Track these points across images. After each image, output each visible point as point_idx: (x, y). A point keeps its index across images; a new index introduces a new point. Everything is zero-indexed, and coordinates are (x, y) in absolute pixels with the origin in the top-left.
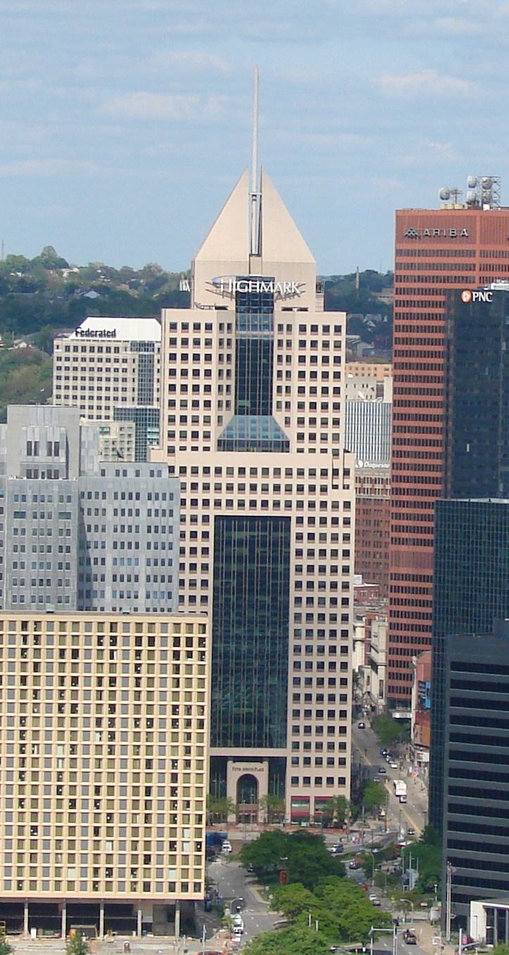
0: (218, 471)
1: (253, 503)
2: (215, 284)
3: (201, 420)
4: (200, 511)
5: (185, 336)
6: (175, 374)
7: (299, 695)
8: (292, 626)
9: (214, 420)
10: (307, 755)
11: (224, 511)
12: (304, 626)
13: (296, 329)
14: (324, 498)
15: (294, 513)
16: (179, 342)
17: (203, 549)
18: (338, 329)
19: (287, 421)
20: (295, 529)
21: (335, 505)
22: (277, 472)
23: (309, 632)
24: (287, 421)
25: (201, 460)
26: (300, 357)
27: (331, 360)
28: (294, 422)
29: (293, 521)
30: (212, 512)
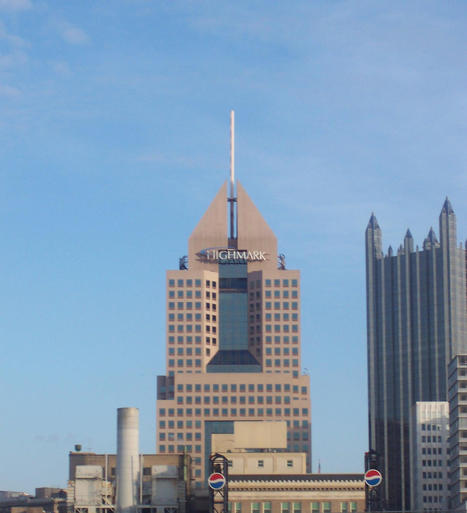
11: (212, 418)
14: (287, 406)
25: (194, 380)
30: (203, 418)
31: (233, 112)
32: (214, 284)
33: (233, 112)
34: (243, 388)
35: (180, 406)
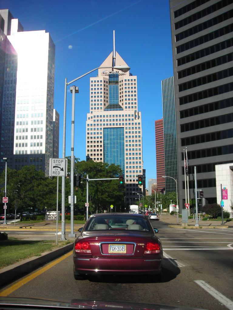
0: (104, 116)
1: (117, 124)
2: (103, 73)
3: (125, 120)
4: (99, 127)
5: (98, 95)
6: (130, 124)
7: (130, 119)
8: (125, 157)
9: (103, 104)
10: (129, 102)
11: (106, 127)
12: (129, 161)
13: (124, 81)
14: (133, 122)
15: (125, 126)
16: (131, 124)
17: (91, 141)
18: (135, 80)
19: (123, 104)
20: (125, 131)
21: (136, 124)
22: (120, 116)
23: (137, 167)
24: (123, 104)
26: (125, 84)
27: (134, 95)
28: (124, 104)
29: (125, 128)
30: (103, 127)
31: (114, 31)
32: (107, 82)
33: (114, 31)
34: (110, 116)
35: (95, 123)
